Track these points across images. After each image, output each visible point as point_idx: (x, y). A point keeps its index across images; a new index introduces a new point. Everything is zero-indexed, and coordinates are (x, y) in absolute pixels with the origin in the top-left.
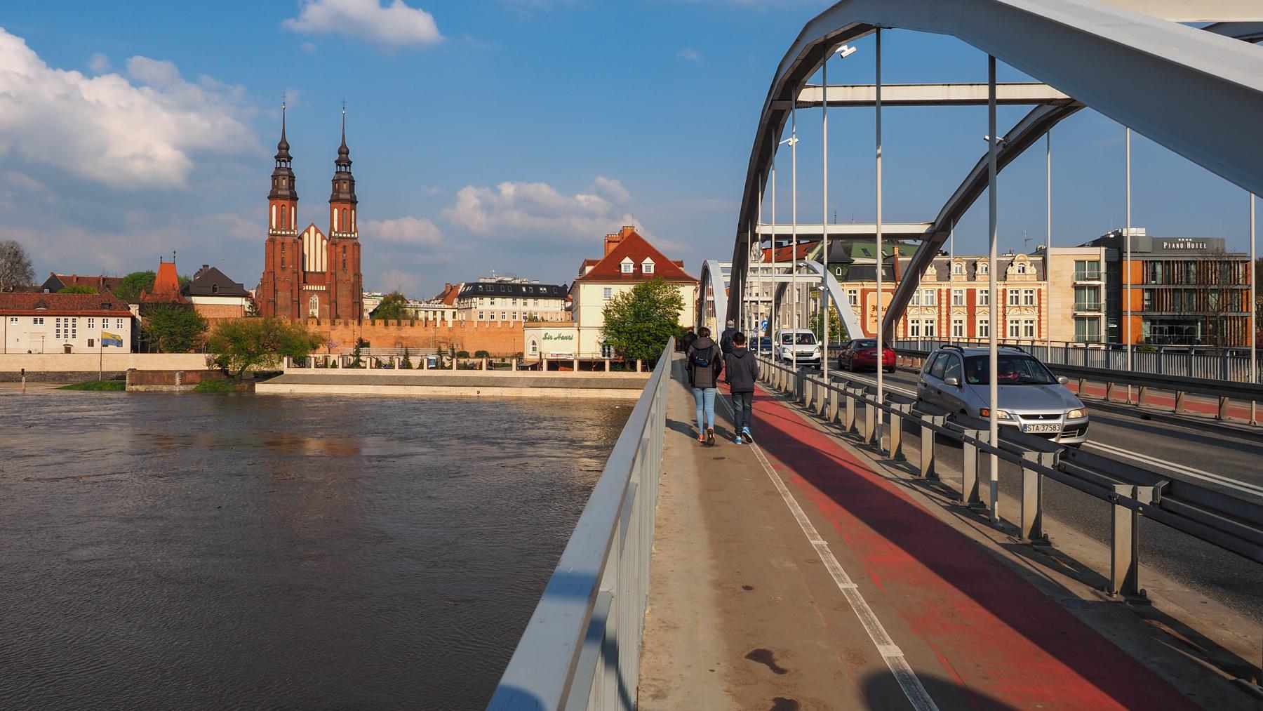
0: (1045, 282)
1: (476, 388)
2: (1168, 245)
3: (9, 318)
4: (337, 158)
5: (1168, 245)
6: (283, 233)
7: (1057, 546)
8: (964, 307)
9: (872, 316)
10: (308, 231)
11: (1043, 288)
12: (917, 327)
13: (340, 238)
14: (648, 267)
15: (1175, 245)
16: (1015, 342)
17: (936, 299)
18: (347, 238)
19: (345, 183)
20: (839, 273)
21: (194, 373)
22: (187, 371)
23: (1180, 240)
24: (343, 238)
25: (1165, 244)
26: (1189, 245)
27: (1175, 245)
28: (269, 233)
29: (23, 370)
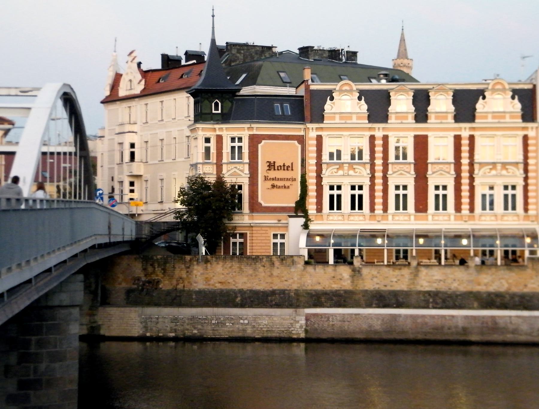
9: (266, 178)
11: (531, 133)
20: (216, 109)
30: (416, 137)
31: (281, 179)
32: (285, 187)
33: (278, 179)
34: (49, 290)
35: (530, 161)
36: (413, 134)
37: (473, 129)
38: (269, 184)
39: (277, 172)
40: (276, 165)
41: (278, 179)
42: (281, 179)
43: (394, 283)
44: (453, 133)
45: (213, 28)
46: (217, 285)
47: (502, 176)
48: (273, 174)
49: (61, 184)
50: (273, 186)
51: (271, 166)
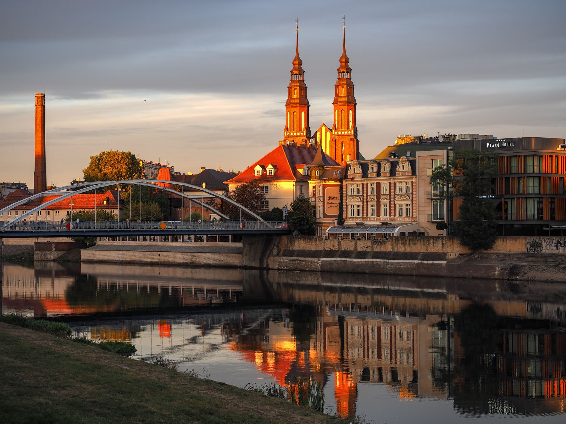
0: (414, 177)
1: (158, 252)
2: (490, 145)
3: (55, 211)
4: (338, 67)
5: (490, 145)
6: (295, 134)
7: (328, 362)
8: (387, 195)
9: (328, 203)
10: (320, 130)
11: (414, 180)
12: (402, 209)
13: (339, 135)
14: (271, 172)
15: (494, 145)
16: (319, 217)
17: (388, 188)
18: (345, 135)
19: (343, 87)
20: (317, 174)
21: (64, 244)
22: (59, 243)
23: (497, 141)
24: (341, 135)
25: (488, 144)
26: (503, 144)
27: (494, 145)
28: (284, 136)
29: (510, 301)
30: (377, 183)
31: (334, 203)
32: (335, 207)
33: (333, 203)
34: (303, 284)
35: (414, 193)
36: (375, 182)
37: (394, 179)
38: (329, 205)
39: (332, 200)
40: (332, 197)
41: (333, 203)
42: (334, 203)
43: (350, 248)
44: (388, 181)
45: (53, 287)
46: (302, 248)
47: (404, 200)
48: (331, 201)
49: (145, 208)
50: (331, 206)
51: (330, 198)
